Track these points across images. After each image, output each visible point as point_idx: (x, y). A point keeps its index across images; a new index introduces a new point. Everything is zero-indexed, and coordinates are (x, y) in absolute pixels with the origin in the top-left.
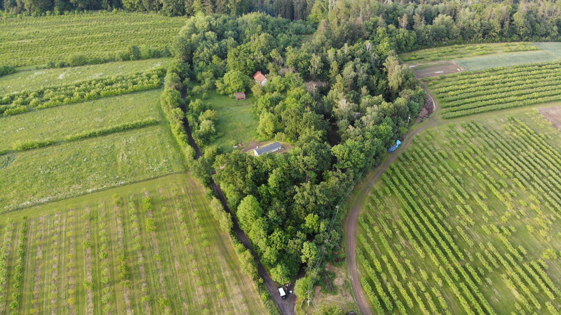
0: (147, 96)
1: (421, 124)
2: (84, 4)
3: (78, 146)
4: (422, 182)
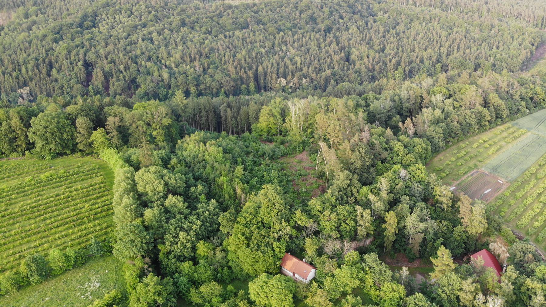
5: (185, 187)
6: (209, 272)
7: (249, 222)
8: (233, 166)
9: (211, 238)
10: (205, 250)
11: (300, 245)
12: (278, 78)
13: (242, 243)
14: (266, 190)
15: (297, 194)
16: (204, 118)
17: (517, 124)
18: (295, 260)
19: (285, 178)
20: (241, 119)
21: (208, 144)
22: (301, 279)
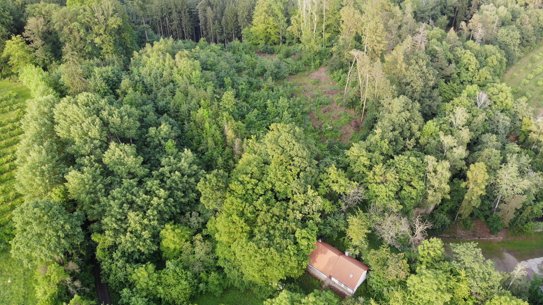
5: (140, 128)
6: (183, 282)
7: (251, 192)
8: (218, 90)
9: (188, 214)
10: (176, 239)
11: (338, 226)
13: (240, 230)
14: (276, 133)
15: (319, 134)
16: (175, 22)
19: (298, 109)
20: (226, 22)
21: (177, 56)
22: (343, 286)
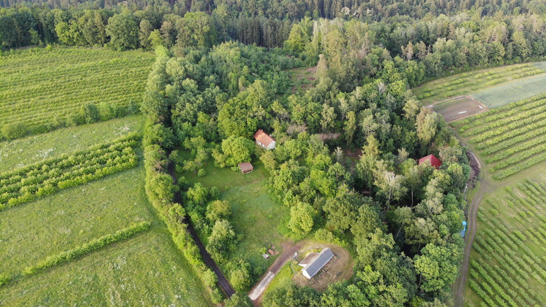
0: (123, 181)
1: (476, 190)
2: (9, 41)
3: (43, 281)
4: (517, 286)
10: (203, 118)
12: (343, 6)
16: (250, 34)
17: (539, 65)
18: (264, 134)
